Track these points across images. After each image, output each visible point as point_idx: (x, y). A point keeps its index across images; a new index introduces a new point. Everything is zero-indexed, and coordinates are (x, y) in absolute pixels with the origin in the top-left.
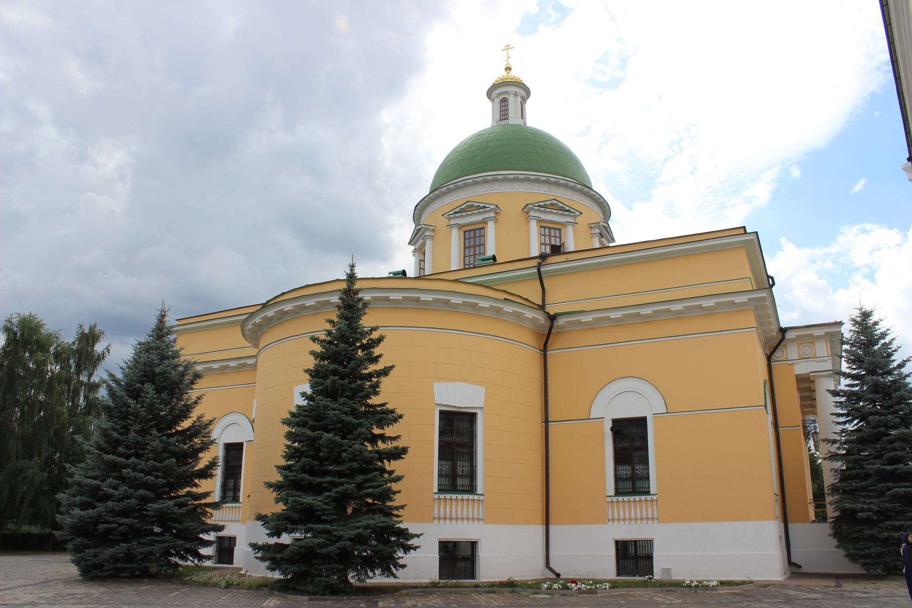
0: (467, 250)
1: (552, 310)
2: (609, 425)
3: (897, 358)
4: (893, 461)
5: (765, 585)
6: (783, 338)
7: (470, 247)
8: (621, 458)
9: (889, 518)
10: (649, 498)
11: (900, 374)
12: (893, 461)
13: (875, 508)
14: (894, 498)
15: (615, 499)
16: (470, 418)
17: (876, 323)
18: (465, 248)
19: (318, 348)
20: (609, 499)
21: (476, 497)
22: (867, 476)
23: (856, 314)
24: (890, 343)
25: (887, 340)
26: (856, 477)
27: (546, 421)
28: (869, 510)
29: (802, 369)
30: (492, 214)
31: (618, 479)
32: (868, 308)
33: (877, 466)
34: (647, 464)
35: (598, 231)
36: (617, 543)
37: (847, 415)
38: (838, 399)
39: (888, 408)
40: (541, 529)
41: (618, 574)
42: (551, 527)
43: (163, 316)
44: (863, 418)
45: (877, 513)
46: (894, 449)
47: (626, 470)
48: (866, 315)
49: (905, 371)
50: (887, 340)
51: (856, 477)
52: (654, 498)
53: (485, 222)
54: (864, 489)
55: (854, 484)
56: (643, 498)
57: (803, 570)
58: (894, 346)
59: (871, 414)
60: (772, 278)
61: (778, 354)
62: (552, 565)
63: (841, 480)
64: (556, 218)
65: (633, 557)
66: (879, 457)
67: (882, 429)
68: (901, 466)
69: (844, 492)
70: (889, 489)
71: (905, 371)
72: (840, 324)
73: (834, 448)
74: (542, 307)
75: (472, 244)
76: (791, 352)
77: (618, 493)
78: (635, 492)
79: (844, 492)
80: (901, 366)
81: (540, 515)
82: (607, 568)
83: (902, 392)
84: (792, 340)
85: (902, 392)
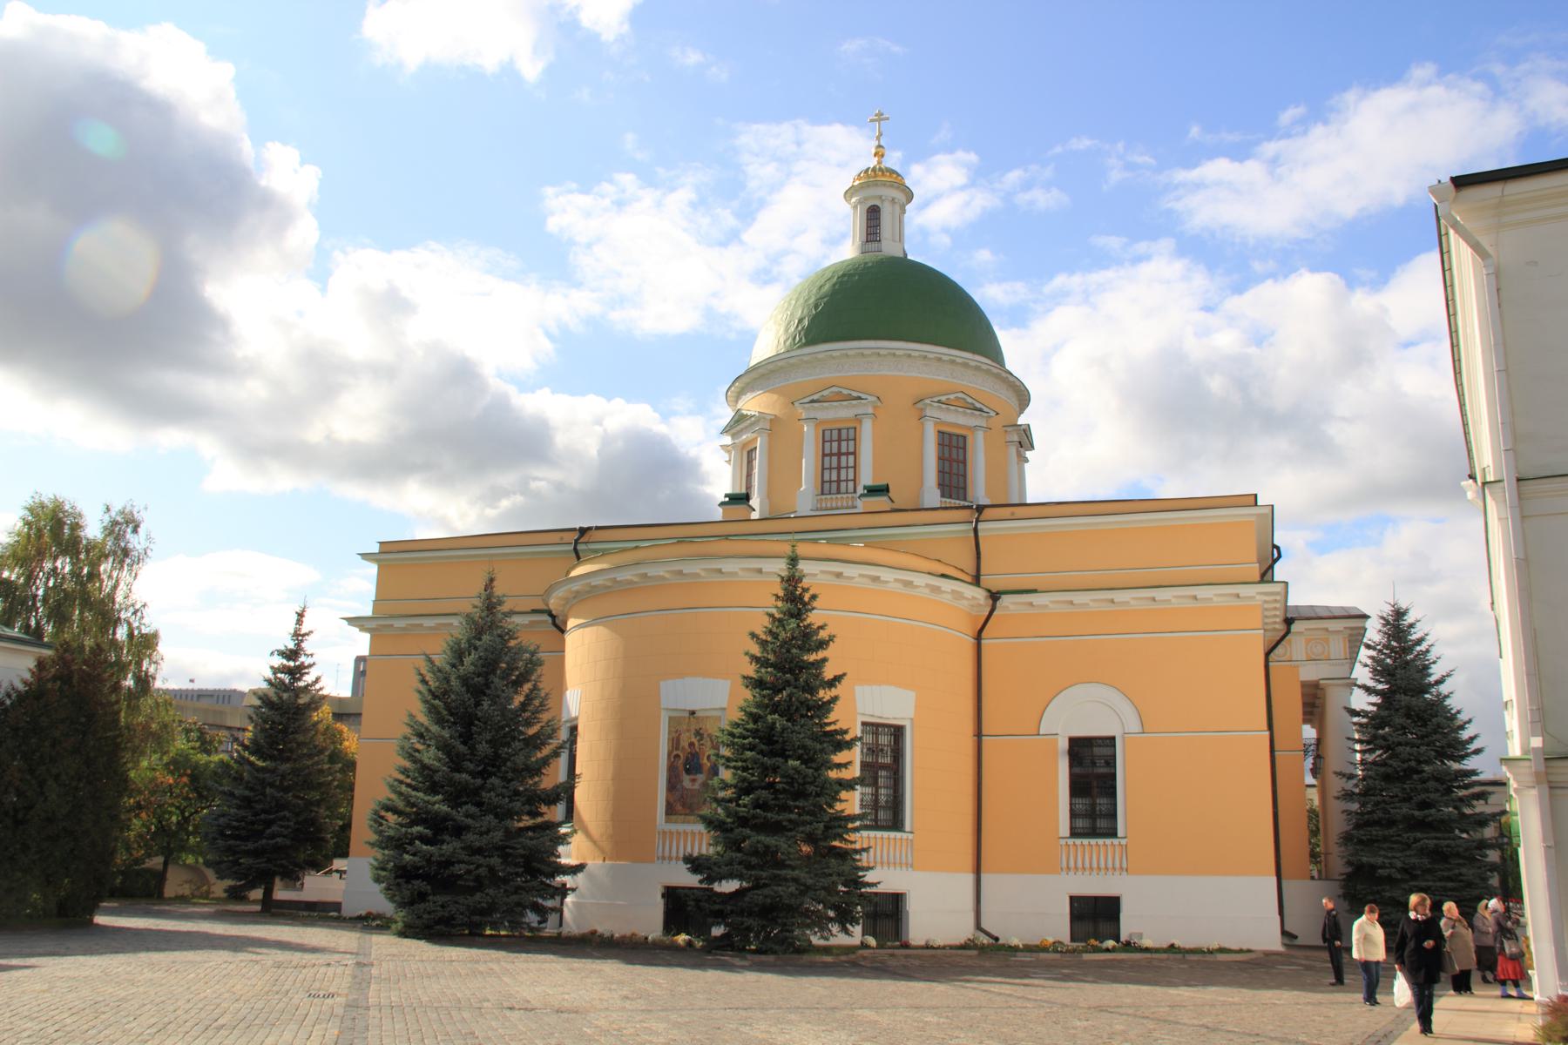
0: (827, 459)
1: (992, 581)
2: (1063, 745)
3: (1436, 672)
4: (1424, 805)
5: (1267, 954)
6: (1288, 632)
7: (831, 455)
8: (1078, 787)
9: (1414, 878)
10: (1115, 841)
11: (1439, 694)
12: (1424, 805)
13: (1399, 864)
14: (1422, 852)
15: (1070, 841)
16: (897, 732)
17: (1411, 626)
18: (824, 455)
19: (756, 650)
20: (1063, 842)
21: (904, 835)
22: (1392, 823)
23: (1387, 610)
24: (1428, 651)
25: (1423, 647)
26: (1377, 823)
27: (979, 734)
28: (1392, 866)
29: (1309, 673)
30: (870, 411)
31: (1073, 815)
32: (1403, 605)
33: (1405, 809)
34: (1113, 794)
35: (1016, 438)
36: (1072, 898)
37: (1368, 743)
38: (1356, 719)
39: (1422, 737)
40: (969, 878)
41: (1073, 939)
42: (983, 876)
43: (492, 580)
44: (1387, 748)
45: (1404, 870)
46: (1427, 791)
47: (1082, 803)
48: (1399, 614)
49: (1444, 689)
50: (1423, 647)
51: (1377, 823)
52: (1123, 842)
53: (858, 419)
54: (1385, 839)
55: (1376, 832)
56: (1108, 841)
57: (1298, 942)
58: (1431, 656)
59: (1400, 744)
60: (1278, 548)
61: (1279, 650)
62: (984, 925)
63: (1357, 826)
64: (961, 420)
65: (1096, 915)
66: (1408, 799)
67: (1413, 764)
68: (1433, 811)
69: (1361, 842)
70: (1416, 840)
71: (1444, 689)
72: (1365, 617)
73: (1350, 785)
74: (976, 581)
75: (835, 450)
76: (1297, 646)
77: (1074, 833)
78: (1093, 833)
79: (1361, 842)
80: (1440, 682)
81: (969, 860)
82: (1058, 927)
83: (1440, 719)
84: (1300, 633)
85: (1440, 719)
